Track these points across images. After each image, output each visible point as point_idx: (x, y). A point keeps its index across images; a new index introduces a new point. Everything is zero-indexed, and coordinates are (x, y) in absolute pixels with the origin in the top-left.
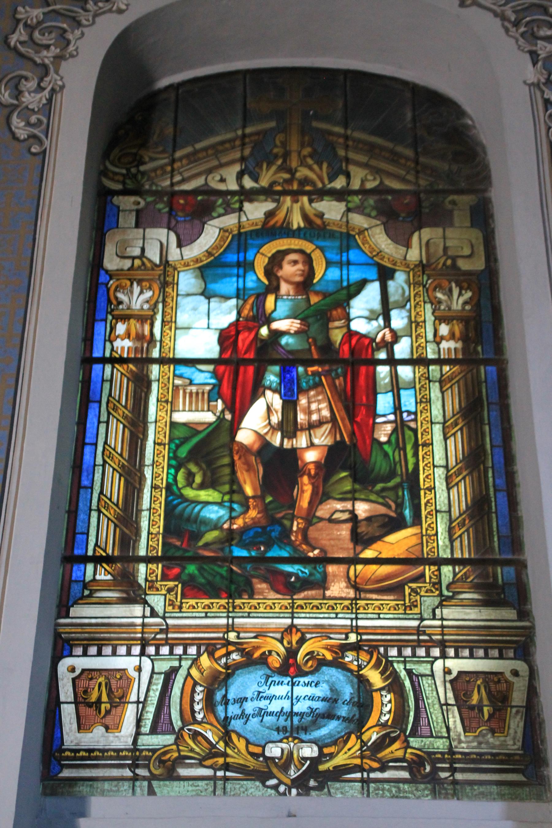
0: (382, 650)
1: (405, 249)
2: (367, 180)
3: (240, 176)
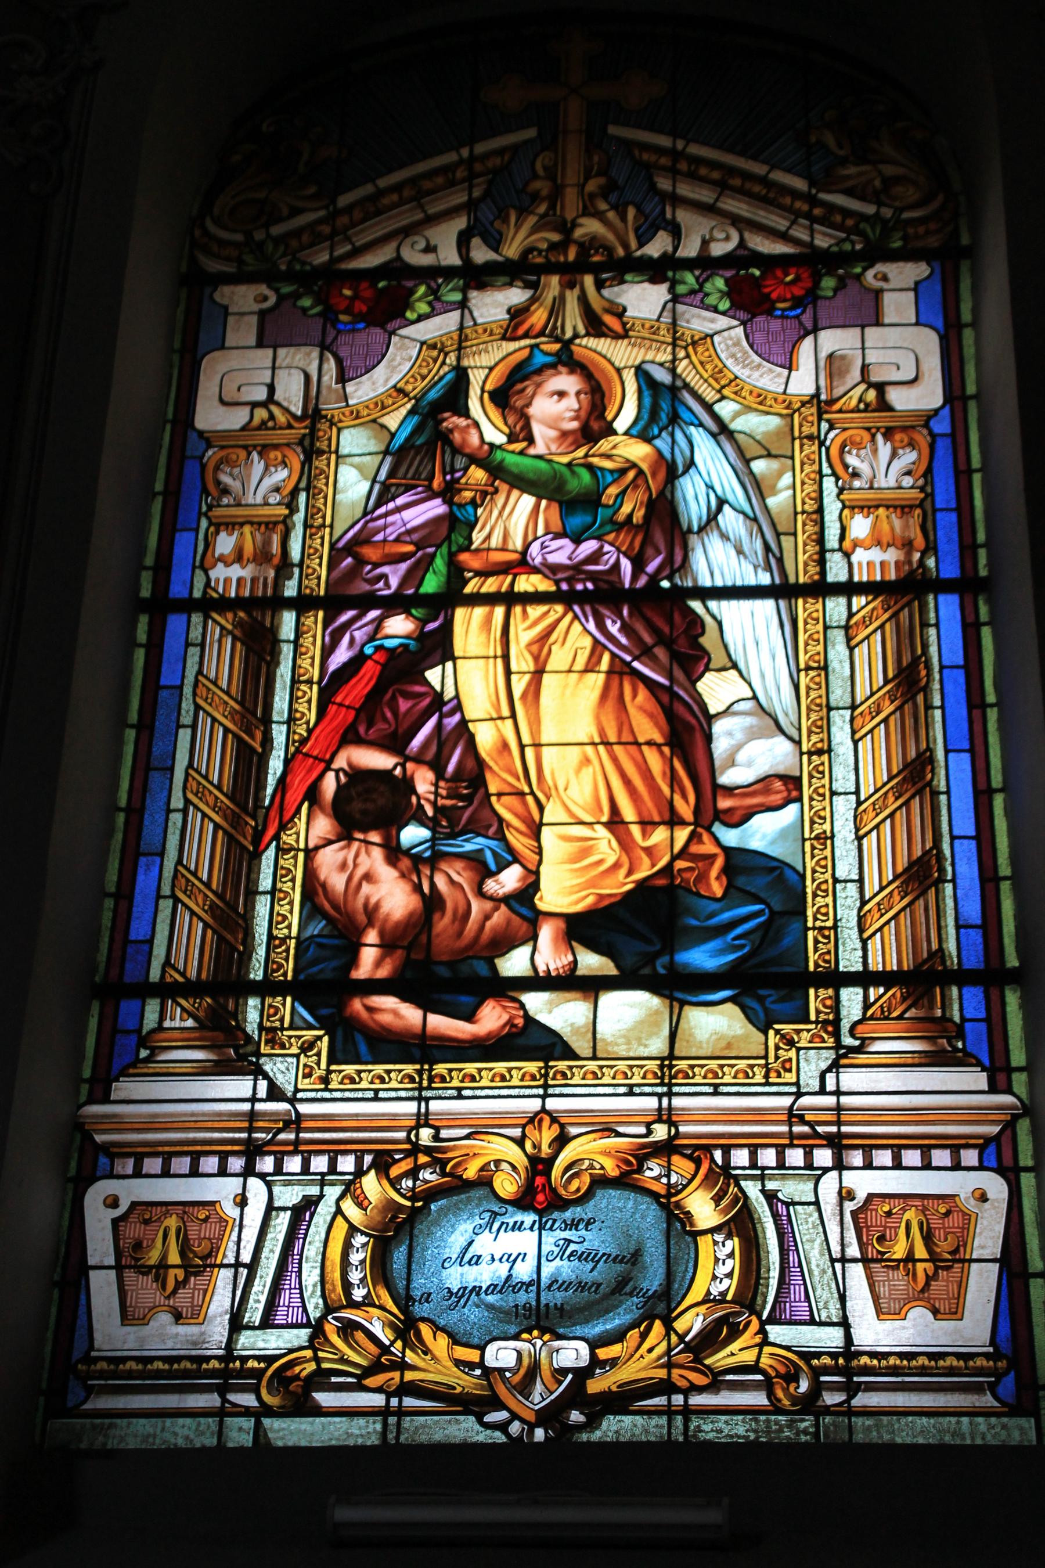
0: (718, 1155)
1: (786, 372)
2: (713, 239)
3: (463, 242)
